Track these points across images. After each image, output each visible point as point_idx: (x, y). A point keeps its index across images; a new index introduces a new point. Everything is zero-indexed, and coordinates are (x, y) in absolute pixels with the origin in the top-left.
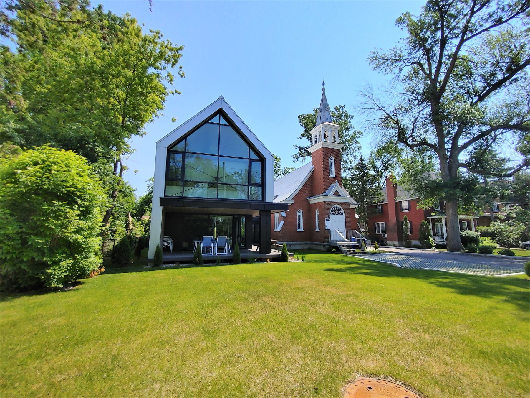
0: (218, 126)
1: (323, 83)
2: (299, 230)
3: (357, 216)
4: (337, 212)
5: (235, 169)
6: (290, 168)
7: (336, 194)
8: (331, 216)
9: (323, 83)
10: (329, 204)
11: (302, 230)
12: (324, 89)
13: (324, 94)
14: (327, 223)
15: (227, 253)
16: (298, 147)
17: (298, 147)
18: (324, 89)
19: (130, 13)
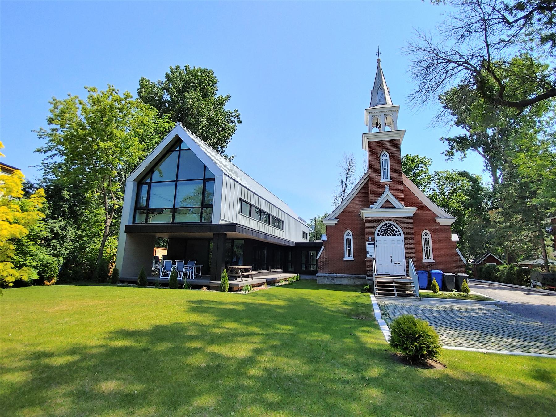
0: (182, 152)
1: (379, 53)
2: (346, 258)
3: (455, 237)
4: (388, 232)
5: (189, 192)
6: (444, 171)
7: (387, 205)
8: (377, 238)
9: (379, 53)
10: (377, 221)
11: (351, 258)
12: (379, 61)
13: (379, 68)
14: (370, 248)
15: (181, 278)
16: (447, 140)
17: (447, 140)
18: (379, 61)
19: (87, 86)
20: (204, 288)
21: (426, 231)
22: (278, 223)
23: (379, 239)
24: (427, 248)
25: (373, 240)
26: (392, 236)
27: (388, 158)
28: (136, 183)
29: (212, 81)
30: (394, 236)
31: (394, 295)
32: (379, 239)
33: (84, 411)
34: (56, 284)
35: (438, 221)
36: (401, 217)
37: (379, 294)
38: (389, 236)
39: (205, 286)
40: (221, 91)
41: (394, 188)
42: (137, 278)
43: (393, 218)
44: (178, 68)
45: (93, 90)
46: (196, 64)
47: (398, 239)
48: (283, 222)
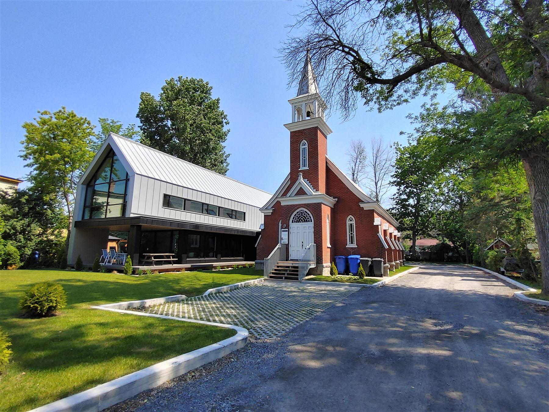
10: (293, 208)
20: (115, 272)
21: (351, 216)
22: (232, 214)
23: (294, 226)
24: (352, 234)
25: (288, 227)
26: (304, 223)
27: (307, 146)
28: (85, 187)
29: (205, 90)
30: (306, 223)
31: (282, 278)
32: (294, 226)
33: (241, 408)
34: (21, 268)
35: (362, 205)
36: (311, 204)
37: (271, 277)
38: (302, 223)
39: (116, 270)
40: (214, 97)
41: (311, 176)
42: (92, 265)
43: (305, 204)
44: (172, 80)
45: (46, 113)
46: (188, 75)
47: (304, 226)
48: (245, 213)
